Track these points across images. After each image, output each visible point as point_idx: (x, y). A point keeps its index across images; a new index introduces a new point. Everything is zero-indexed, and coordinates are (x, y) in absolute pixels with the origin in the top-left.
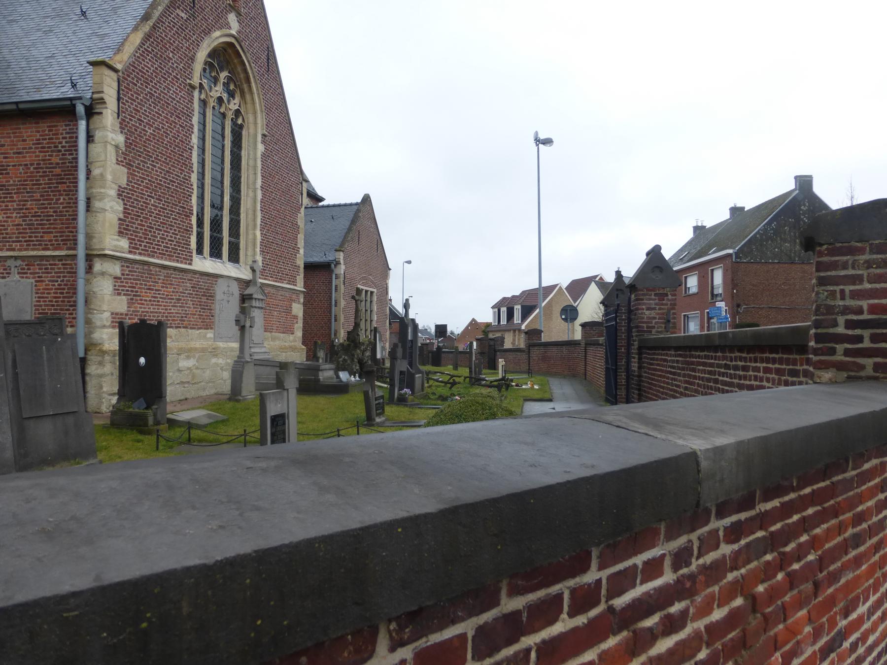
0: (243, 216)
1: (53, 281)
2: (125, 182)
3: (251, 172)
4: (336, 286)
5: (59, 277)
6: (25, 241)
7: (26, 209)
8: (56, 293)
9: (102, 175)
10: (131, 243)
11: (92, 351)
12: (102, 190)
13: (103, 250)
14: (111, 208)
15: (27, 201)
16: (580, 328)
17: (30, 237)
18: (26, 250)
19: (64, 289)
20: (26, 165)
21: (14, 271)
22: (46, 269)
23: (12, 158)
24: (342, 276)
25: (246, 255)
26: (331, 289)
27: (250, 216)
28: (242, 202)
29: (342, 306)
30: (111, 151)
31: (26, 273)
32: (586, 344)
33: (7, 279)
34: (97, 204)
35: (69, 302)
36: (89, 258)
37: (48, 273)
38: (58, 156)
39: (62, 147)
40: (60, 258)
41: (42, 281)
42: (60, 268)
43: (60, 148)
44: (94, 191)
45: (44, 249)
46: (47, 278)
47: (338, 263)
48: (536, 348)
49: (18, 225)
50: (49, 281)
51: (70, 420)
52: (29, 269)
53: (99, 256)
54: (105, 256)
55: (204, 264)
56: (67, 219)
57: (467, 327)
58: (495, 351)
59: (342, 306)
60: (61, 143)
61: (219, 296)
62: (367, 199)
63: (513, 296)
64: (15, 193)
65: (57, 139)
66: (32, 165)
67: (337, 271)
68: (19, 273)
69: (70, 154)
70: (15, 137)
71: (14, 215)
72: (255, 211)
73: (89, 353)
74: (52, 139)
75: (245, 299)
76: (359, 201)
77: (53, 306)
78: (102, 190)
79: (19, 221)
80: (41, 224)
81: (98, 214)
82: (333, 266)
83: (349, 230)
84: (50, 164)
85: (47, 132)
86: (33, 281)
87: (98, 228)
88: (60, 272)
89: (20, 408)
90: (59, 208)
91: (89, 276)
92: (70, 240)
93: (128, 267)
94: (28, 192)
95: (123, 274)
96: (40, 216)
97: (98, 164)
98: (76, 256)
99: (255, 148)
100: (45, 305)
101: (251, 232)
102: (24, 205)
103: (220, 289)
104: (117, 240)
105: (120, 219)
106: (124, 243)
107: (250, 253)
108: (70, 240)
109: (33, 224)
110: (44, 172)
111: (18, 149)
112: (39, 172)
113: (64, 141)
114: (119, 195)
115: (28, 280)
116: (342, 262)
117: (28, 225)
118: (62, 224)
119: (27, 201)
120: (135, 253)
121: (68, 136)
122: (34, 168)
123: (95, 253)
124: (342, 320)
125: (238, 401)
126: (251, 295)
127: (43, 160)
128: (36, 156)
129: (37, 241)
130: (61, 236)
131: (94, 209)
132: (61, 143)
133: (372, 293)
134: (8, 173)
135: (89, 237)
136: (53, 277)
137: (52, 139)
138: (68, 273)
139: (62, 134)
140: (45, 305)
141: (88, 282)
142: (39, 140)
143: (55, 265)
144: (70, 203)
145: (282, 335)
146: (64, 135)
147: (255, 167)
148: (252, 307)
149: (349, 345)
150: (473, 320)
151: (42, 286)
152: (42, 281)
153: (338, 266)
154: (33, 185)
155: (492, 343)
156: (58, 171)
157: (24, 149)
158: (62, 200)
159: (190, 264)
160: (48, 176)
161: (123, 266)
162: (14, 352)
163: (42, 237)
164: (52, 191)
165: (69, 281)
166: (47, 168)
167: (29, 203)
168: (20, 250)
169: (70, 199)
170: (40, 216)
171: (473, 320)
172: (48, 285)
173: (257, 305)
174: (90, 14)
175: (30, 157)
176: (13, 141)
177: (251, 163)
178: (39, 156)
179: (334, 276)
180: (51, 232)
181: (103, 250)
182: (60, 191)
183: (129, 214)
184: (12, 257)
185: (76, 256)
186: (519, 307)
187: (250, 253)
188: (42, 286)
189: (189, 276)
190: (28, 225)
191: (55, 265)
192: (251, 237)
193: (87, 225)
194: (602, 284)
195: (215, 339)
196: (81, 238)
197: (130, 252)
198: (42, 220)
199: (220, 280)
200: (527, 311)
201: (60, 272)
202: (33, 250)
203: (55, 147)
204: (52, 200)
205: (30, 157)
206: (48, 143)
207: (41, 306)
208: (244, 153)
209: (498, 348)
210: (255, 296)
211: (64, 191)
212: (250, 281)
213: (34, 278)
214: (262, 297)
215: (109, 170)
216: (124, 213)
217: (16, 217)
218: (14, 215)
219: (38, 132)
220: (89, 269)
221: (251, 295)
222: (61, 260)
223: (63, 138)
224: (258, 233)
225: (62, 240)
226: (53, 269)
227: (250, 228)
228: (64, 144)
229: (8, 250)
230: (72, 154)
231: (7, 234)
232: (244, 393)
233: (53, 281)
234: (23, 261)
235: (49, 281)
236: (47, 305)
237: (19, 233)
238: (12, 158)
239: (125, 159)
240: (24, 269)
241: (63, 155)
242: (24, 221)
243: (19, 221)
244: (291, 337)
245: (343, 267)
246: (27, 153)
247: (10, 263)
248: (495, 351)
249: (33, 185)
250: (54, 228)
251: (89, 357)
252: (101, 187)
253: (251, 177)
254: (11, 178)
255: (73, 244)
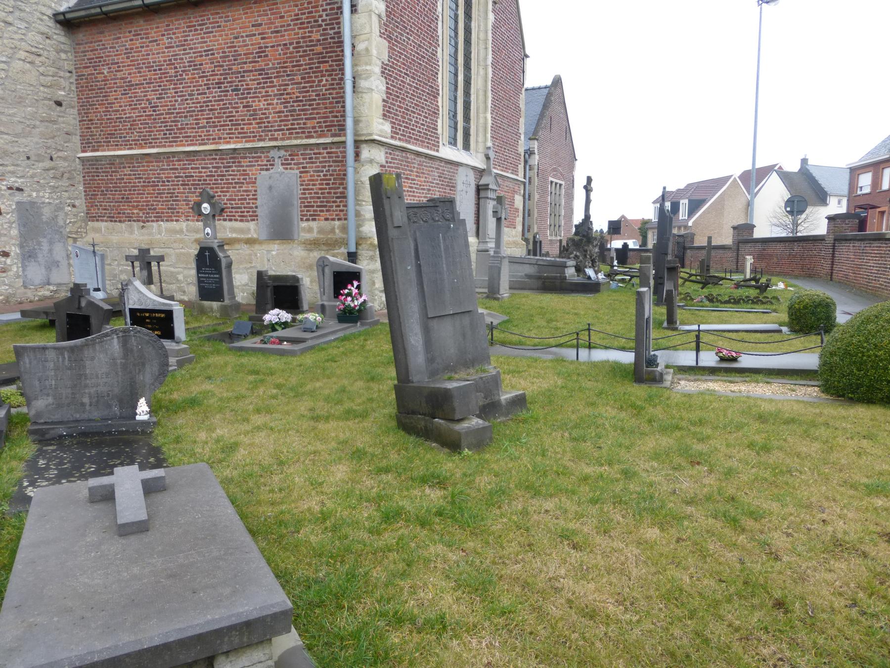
0: (473, 98)
1: (318, 171)
2: (387, 58)
3: (482, 46)
5: (324, 167)
6: (288, 129)
7: (287, 94)
8: (322, 184)
9: (367, 50)
10: (392, 127)
11: (363, 245)
12: (368, 68)
13: (371, 134)
14: (377, 87)
15: (288, 85)
16: (827, 221)
17: (292, 124)
18: (289, 139)
19: (330, 180)
20: (285, 45)
21: (278, 162)
22: (310, 158)
23: (270, 38)
24: (536, 167)
25: (477, 142)
27: (481, 97)
28: (472, 82)
29: (536, 200)
30: (375, 19)
31: (290, 164)
32: (835, 240)
33: (271, 171)
34: (363, 84)
35: (335, 193)
36: (357, 143)
37: (312, 163)
38: (318, 31)
39: (323, 21)
40: (325, 146)
41: (307, 172)
42: (325, 157)
43: (320, 22)
44: (359, 68)
45: (307, 137)
46: (311, 168)
48: (750, 245)
49: (280, 112)
50: (314, 171)
51: (466, 320)
52: (292, 160)
53: (366, 141)
54: (373, 141)
55: (447, 152)
56: (331, 103)
58: (685, 248)
59: (536, 200)
60: (321, 16)
61: (460, 187)
62: (557, 82)
63: (679, 190)
64: (275, 77)
65: (316, 12)
66: (291, 44)
68: (282, 164)
69: (331, 29)
70: (272, 14)
71: (276, 101)
72: (485, 92)
73: (360, 247)
74: (312, 12)
76: (549, 83)
77: (319, 198)
78: (368, 68)
79: (280, 107)
80: (303, 110)
81: (364, 95)
83: (542, 115)
84: (311, 41)
86: (297, 171)
87: (365, 110)
88: (326, 162)
89: (425, 306)
90: (321, 90)
91: (357, 165)
92: (335, 126)
93: (390, 154)
94: (288, 75)
95: (387, 162)
96: (301, 101)
97: (362, 37)
98: (344, 142)
99: (486, 18)
100: (311, 198)
101: (481, 115)
102: (285, 90)
104: (382, 124)
105: (384, 101)
106: (387, 127)
107: (481, 139)
108: (335, 126)
109: (294, 111)
110: (304, 51)
111: (276, 27)
112: (299, 52)
113: (324, 13)
114: (383, 72)
115: (292, 171)
116: (536, 151)
117: (290, 111)
118: (326, 108)
119: (288, 85)
120: (396, 139)
121: (328, 7)
122: (294, 48)
123: (363, 138)
124: (536, 215)
125: (497, 299)
126: (488, 185)
127: (303, 38)
128: (295, 34)
129: (300, 128)
130: (325, 122)
131: (360, 90)
132: (321, 16)
133: (561, 185)
134: (266, 56)
135: (356, 122)
136: (318, 167)
137: (312, 12)
138: (333, 161)
139: (322, 6)
140: (311, 198)
141: (356, 171)
142: (298, 15)
143: (320, 153)
144: (333, 84)
146: (325, 7)
147: (486, 40)
148: (487, 198)
149: (581, 240)
151: (307, 177)
152: (307, 172)
153: (532, 156)
154: (293, 66)
155: (681, 240)
156: (319, 49)
157: (281, 26)
158: (324, 82)
159: (438, 151)
160: (309, 55)
161: (386, 153)
162: (415, 240)
163: (304, 124)
164: (313, 72)
165: (335, 171)
166: (307, 46)
167: (290, 87)
168: (282, 139)
169: (333, 79)
170: (301, 101)
172: (313, 176)
175: (289, 35)
176: (270, 19)
177: (482, 36)
178: (298, 34)
180: (315, 118)
181: (371, 134)
182: (322, 71)
183: (391, 94)
184: (275, 147)
185: (344, 142)
186: (686, 201)
187: (481, 139)
188: (307, 177)
190: (290, 111)
191: (320, 153)
192: (481, 121)
193: (354, 108)
194: (785, 177)
196: (349, 123)
197: (392, 137)
198: (304, 105)
199: (461, 169)
200: (694, 206)
201: (326, 162)
202: (296, 138)
203: (315, 21)
204: (314, 82)
205: (289, 35)
206: (307, 18)
207: (306, 198)
208: (474, 25)
209: (687, 245)
210: (490, 187)
211: (327, 71)
212: (484, 170)
213: (298, 168)
215: (374, 43)
216: (387, 93)
217: (277, 103)
218: (276, 101)
219: (297, 6)
220: (357, 155)
221: (488, 185)
222: (326, 148)
223: (323, 10)
224: (489, 116)
225: (326, 127)
226: (318, 158)
228: (324, 17)
229: (270, 140)
230: (334, 28)
231: (269, 122)
232: (502, 292)
233: (318, 171)
234: (286, 151)
235: (314, 171)
236: (313, 198)
237: (281, 121)
238: (270, 38)
239: (386, 30)
240: (287, 160)
241: (324, 30)
242: (285, 107)
243: (280, 107)
244: (514, 232)
245: (537, 157)
246: (285, 31)
247: (272, 153)
248: (685, 248)
249: (293, 66)
250: (318, 113)
251: (359, 252)
252: (367, 64)
253: (482, 52)
254: (270, 60)
255: (342, 128)
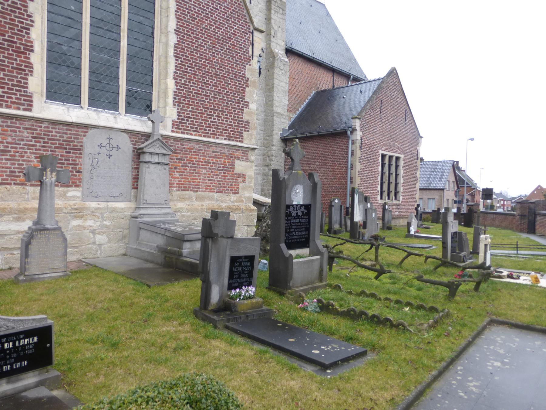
4: (352, 151)
26: (347, 154)
47: (354, 130)
57: (533, 192)
62: (393, 73)
67: (353, 137)
75: (138, 154)
82: (349, 132)
85: (194, 64)
103: (90, 144)
116: (358, 128)
133: (398, 159)
145: (216, 195)
150: (539, 186)
153: (355, 133)
155: (532, 206)
159: (30, 110)
171: (539, 186)
173: (157, 160)
174: (299, 21)
179: (350, 142)
189: (27, 124)
195: (84, 198)
199: (91, 132)
214: (164, 152)
227: (162, 77)
